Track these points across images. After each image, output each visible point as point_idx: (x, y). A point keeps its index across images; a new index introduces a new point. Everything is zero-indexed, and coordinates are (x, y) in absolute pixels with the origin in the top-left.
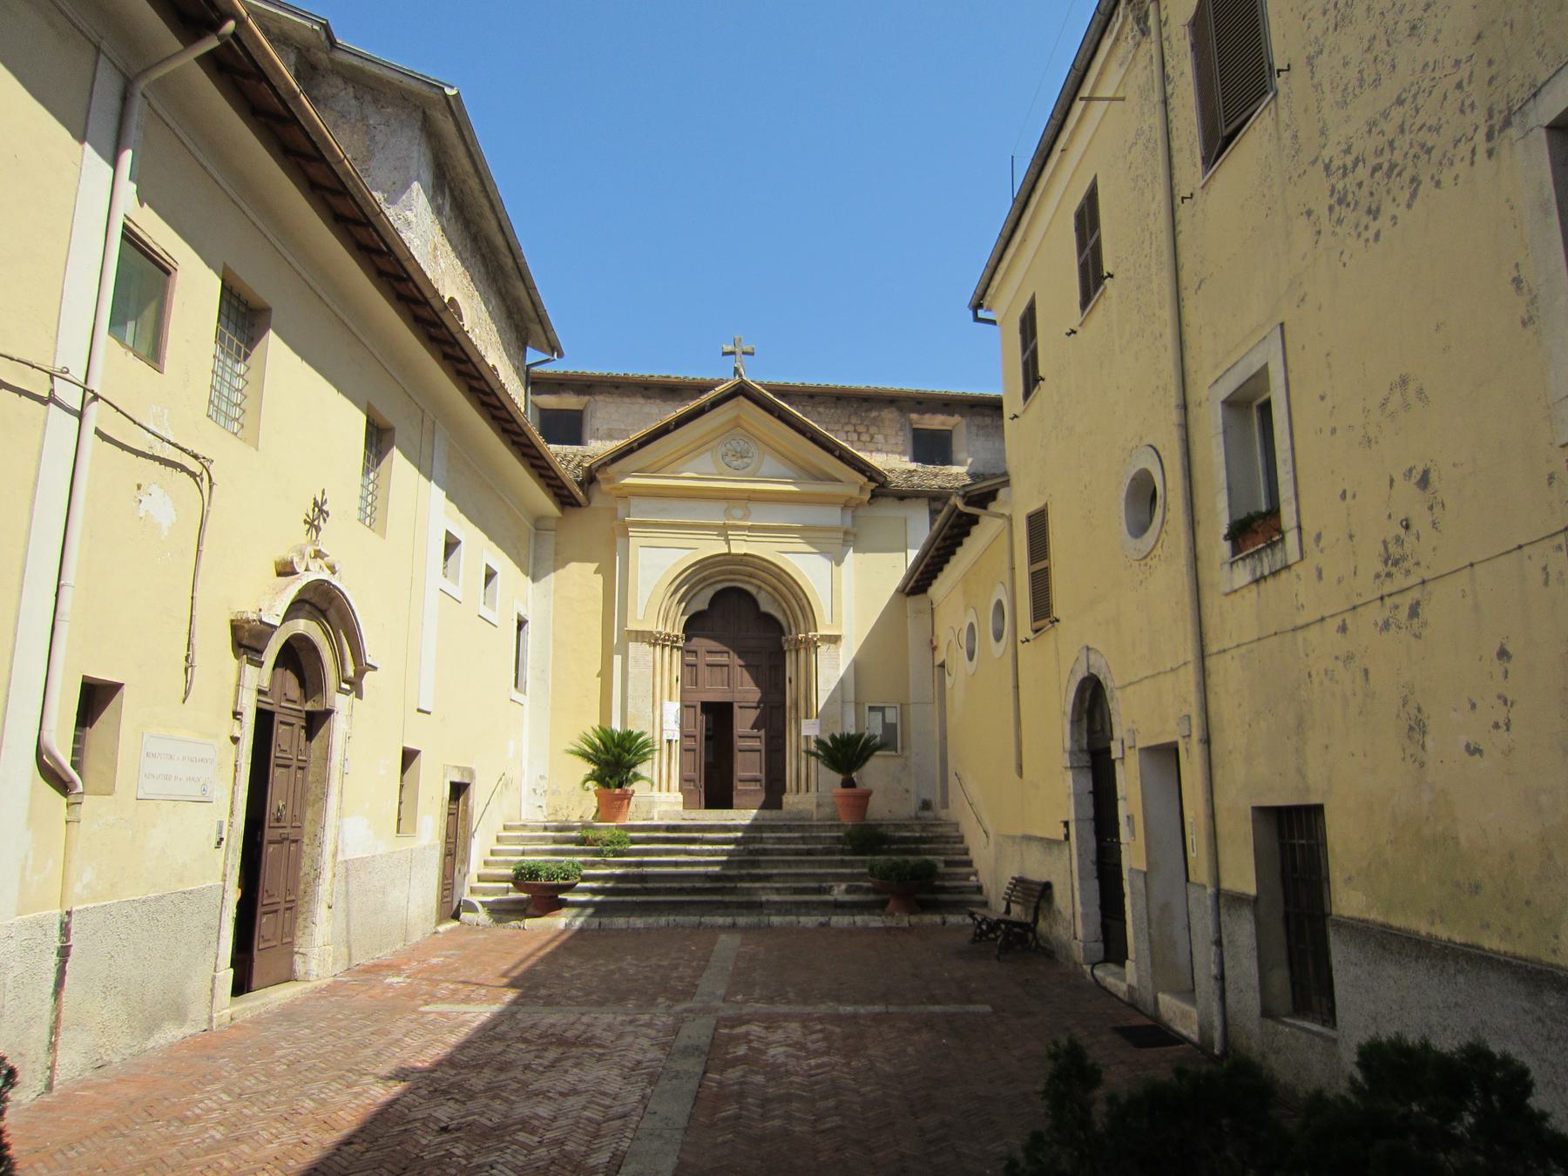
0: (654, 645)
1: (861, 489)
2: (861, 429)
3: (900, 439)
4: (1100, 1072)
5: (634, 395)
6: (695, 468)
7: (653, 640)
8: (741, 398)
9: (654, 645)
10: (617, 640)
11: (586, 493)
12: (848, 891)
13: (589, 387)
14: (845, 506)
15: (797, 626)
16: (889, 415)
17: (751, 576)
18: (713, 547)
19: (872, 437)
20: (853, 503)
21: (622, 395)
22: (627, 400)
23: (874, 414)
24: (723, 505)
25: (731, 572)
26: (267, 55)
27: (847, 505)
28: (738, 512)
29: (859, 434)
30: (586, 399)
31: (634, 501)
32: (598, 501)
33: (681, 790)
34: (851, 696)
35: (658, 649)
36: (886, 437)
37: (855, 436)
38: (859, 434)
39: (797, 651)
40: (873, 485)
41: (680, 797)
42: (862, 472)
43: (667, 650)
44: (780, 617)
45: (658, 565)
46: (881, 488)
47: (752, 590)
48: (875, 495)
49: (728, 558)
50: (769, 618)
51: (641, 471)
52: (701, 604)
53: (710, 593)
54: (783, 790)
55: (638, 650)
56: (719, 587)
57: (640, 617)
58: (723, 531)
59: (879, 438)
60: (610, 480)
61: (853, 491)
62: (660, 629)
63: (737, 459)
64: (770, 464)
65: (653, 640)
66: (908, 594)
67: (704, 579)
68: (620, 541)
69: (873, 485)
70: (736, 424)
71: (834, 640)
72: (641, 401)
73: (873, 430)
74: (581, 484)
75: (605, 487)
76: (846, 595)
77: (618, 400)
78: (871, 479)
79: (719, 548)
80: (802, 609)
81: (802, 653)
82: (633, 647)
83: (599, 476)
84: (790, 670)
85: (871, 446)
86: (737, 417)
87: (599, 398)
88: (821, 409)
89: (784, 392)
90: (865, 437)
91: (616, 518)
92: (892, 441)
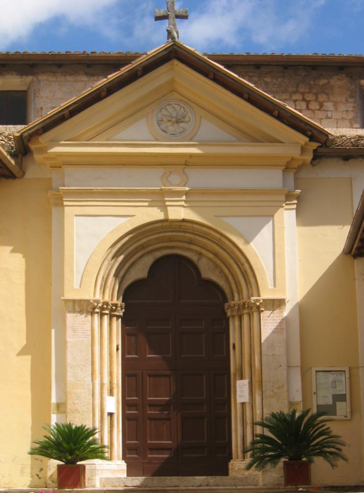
0: (92, 313)
1: (303, 150)
2: (310, 97)
3: (350, 106)
4: (69, 427)
5: (74, 73)
6: (130, 134)
7: (87, 308)
8: (176, 62)
9: (92, 313)
10: (45, 307)
11: (20, 165)
12: (111, 393)
13: (33, 66)
14: (287, 168)
15: (240, 292)
16: (338, 82)
17: (191, 242)
18: (146, 214)
19: (321, 105)
20: (295, 164)
21: (65, 74)
22: (69, 78)
23: (323, 82)
24: (160, 171)
25: (170, 240)
26: (265, 95)
27: (288, 167)
28: (175, 178)
29: (308, 102)
30: (29, 79)
31: (68, 170)
32: (32, 172)
33: (124, 458)
34: (296, 360)
35: (96, 317)
36: (336, 104)
37: (303, 105)
38: (308, 102)
39: (241, 318)
40: (315, 145)
41: (123, 465)
42: (303, 132)
43: (106, 319)
44: (221, 283)
45: (92, 237)
46: (325, 150)
47: (194, 257)
48: (317, 157)
49: (165, 226)
50: (211, 285)
51: (75, 140)
52: (140, 272)
53: (149, 261)
54: (230, 457)
55: (78, 323)
56: (159, 254)
57: (76, 285)
58: (158, 198)
59: (329, 105)
60: (43, 150)
61: (295, 152)
62: (98, 296)
63: (175, 126)
64: (209, 129)
65: (87, 308)
66: (355, 256)
67: (143, 247)
68: (54, 210)
69: (315, 145)
70: (171, 88)
71: (278, 304)
72: (85, 78)
73: (322, 97)
74: (14, 156)
75: (37, 157)
76: (290, 258)
77: (62, 78)
78: (312, 138)
79: (154, 214)
80: (244, 274)
81: (246, 318)
82: (70, 317)
83: (32, 146)
84: (234, 338)
85: (320, 114)
86: (172, 82)
87: (43, 77)
88: (268, 79)
89: (231, 62)
90: (314, 106)
91: (51, 188)
92: (342, 108)
